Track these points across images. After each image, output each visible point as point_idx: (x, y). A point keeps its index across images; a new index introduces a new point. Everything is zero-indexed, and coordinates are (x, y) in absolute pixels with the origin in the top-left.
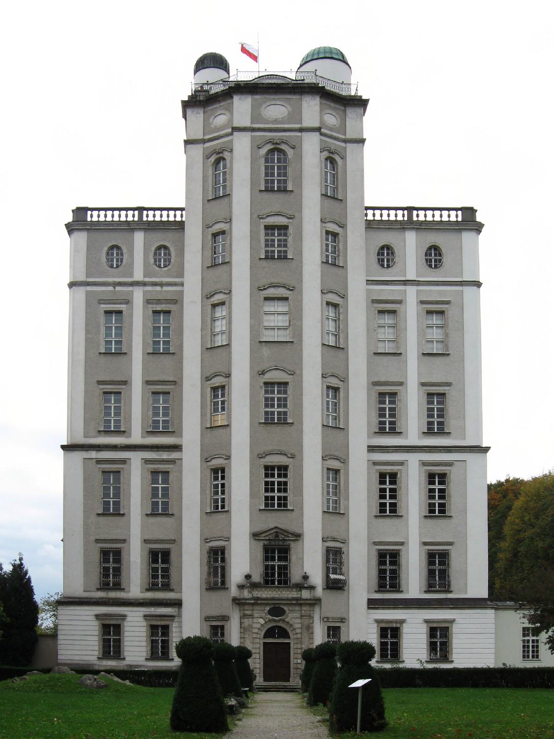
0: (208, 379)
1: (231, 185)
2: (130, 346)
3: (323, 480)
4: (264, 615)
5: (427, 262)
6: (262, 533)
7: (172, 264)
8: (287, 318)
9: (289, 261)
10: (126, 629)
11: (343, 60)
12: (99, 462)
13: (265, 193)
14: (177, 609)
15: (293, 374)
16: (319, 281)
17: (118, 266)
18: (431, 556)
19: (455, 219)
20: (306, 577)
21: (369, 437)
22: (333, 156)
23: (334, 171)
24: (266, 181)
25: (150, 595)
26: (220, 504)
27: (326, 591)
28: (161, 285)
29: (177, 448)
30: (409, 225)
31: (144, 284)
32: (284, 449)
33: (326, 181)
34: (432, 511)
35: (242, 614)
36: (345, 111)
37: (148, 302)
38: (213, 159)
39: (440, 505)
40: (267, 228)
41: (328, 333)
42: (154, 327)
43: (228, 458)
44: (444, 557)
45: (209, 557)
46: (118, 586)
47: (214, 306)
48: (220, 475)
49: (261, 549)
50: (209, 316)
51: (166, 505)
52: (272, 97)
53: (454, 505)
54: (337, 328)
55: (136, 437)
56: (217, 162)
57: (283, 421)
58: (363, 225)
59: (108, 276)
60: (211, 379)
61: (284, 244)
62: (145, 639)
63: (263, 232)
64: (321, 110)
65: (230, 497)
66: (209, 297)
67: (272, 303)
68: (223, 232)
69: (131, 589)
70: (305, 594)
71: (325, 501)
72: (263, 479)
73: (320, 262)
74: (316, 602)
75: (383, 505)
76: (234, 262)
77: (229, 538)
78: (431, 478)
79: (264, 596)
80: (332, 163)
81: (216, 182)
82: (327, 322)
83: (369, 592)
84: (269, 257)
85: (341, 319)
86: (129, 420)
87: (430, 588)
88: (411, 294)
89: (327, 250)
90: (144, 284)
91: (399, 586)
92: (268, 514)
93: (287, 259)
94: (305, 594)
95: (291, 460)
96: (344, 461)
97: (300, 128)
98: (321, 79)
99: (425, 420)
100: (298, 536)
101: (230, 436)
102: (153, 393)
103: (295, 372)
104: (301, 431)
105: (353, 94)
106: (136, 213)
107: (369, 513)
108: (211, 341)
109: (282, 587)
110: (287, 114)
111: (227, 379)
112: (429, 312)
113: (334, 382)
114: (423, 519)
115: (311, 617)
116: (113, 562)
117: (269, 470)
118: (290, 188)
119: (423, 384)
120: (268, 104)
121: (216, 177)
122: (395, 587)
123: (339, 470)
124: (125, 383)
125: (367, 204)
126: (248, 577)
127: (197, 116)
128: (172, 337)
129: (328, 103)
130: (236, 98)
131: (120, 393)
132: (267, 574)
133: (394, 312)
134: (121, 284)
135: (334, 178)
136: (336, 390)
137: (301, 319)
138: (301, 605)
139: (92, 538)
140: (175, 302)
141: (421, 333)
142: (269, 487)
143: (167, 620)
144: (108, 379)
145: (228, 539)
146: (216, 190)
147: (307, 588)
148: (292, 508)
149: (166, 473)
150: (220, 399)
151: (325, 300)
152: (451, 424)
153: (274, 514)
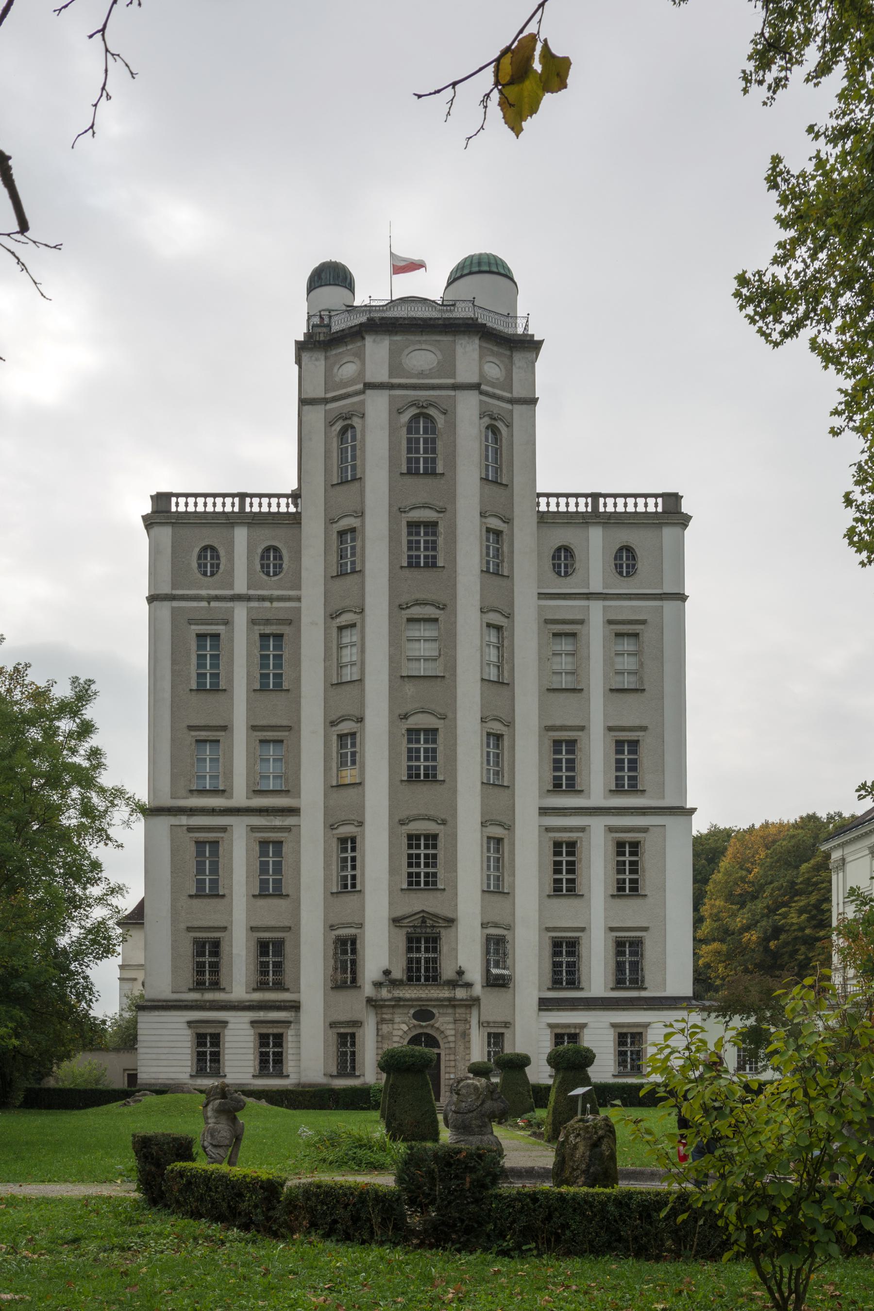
0: (333, 724)
1: (363, 465)
2: (231, 681)
3: (482, 852)
4: (407, 1019)
5: (616, 568)
6: (407, 917)
7: (284, 572)
8: (435, 645)
9: (440, 570)
10: (227, 1039)
11: (508, 276)
12: (190, 829)
13: (407, 477)
14: (293, 1014)
15: (443, 718)
16: (478, 597)
17: (213, 574)
18: (620, 945)
19: (654, 510)
20: (460, 973)
21: (540, 797)
22: (496, 423)
23: (496, 444)
24: (409, 460)
25: (257, 996)
26: (349, 882)
27: (486, 989)
28: (271, 599)
29: (294, 811)
30: (594, 518)
31: (248, 598)
32: (432, 813)
33: (487, 459)
34: (621, 889)
35: (379, 1019)
36: (511, 357)
37: (253, 622)
38: (338, 426)
39: (632, 881)
40: (410, 524)
41: (489, 665)
42: (261, 655)
43: (361, 824)
44: (636, 945)
45: (336, 948)
46: (216, 986)
47: (341, 629)
48: (349, 845)
49: (404, 938)
50: (335, 642)
51: (278, 883)
52: (418, 338)
53: (648, 880)
54: (500, 657)
55: (240, 797)
56: (344, 431)
57: (430, 776)
58: (535, 519)
59: (200, 588)
60: (337, 724)
61: (432, 546)
62: (252, 1051)
63: (404, 530)
64: (481, 357)
65: (363, 874)
66: (333, 616)
67: (416, 626)
68: (353, 530)
69: (234, 989)
70: (460, 993)
71: (485, 878)
72: (405, 851)
73: (478, 571)
74: (474, 1002)
75: (557, 881)
76: (367, 572)
77: (362, 924)
78: (620, 846)
79: (408, 996)
80: (494, 433)
81: (343, 459)
82: (487, 650)
83: (540, 990)
84: (413, 563)
85: (505, 645)
86: (229, 774)
87: (619, 983)
88: (596, 612)
89: (488, 554)
90: (248, 598)
91: (579, 983)
92: (413, 895)
93: (436, 567)
94: (460, 993)
95: (442, 827)
96: (509, 827)
97: (453, 384)
98: (480, 311)
99: (613, 774)
100: (451, 922)
101: (364, 796)
102: (261, 741)
103: (447, 716)
104: (455, 791)
105: (520, 331)
106: (237, 500)
107: (541, 890)
108: (338, 674)
109: (431, 985)
110: (435, 364)
111: (359, 724)
112: (618, 635)
113: (497, 727)
114: (610, 899)
115: (466, 1021)
116: (210, 956)
117: (413, 840)
118: (440, 470)
119: (610, 729)
120: (411, 349)
121: (343, 452)
122: (573, 983)
123: (502, 839)
124: (224, 728)
125: (538, 491)
126: (387, 973)
127: (317, 363)
128: (286, 670)
129: (490, 346)
130: (369, 340)
131: (218, 741)
132: (409, 969)
133: (574, 635)
134: (217, 598)
135: (496, 454)
136: (499, 737)
137: (455, 646)
138: (454, 1006)
139: (183, 926)
140: (289, 622)
141: (608, 662)
142: (413, 860)
143: (281, 1027)
144: (202, 722)
145: (361, 926)
146: (342, 470)
147: (462, 986)
148: (442, 887)
149: (279, 844)
150: (349, 750)
151: (485, 620)
152: (646, 778)
153: (420, 895)
